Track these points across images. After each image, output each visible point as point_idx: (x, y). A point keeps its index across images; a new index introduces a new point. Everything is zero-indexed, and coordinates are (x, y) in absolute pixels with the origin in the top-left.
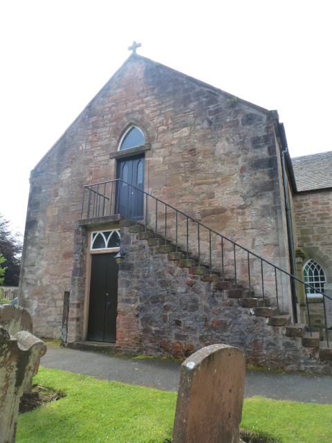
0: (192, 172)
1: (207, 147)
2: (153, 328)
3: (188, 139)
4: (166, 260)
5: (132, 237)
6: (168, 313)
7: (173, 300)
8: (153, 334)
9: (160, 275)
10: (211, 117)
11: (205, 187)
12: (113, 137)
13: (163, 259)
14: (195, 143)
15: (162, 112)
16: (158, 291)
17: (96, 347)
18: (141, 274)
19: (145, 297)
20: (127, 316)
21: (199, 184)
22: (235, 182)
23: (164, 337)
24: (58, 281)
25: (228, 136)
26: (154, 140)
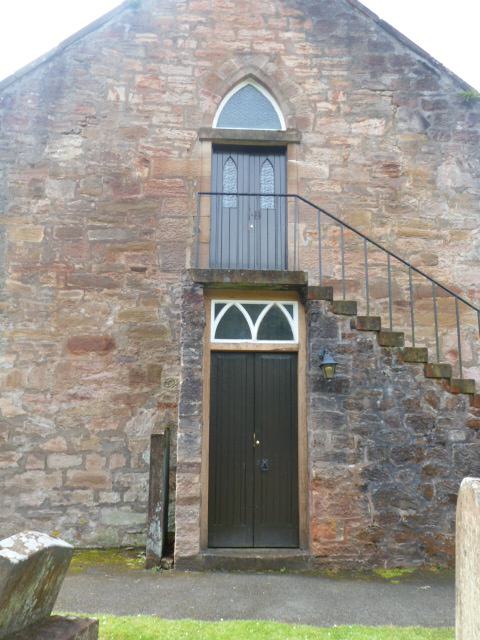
0: (393, 209)
1: (421, 168)
2: (402, 513)
3: (382, 142)
4: (420, 377)
5: (339, 324)
6: (434, 482)
7: (440, 456)
8: (403, 525)
9: (411, 405)
10: (426, 114)
11: (419, 243)
12: (208, 94)
13: (414, 373)
14: (396, 153)
15: (324, 73)
16: (409, 436)
17: (262, 561)
18: (366, 402)
19: (380, 450)
20: (337, 490)
21: (408, 235)
22: (474, 243)
23: (429, 529)
24: (54, 408)
25: (460, 156)
26: (307, 126)
